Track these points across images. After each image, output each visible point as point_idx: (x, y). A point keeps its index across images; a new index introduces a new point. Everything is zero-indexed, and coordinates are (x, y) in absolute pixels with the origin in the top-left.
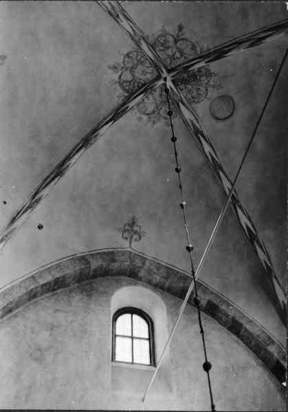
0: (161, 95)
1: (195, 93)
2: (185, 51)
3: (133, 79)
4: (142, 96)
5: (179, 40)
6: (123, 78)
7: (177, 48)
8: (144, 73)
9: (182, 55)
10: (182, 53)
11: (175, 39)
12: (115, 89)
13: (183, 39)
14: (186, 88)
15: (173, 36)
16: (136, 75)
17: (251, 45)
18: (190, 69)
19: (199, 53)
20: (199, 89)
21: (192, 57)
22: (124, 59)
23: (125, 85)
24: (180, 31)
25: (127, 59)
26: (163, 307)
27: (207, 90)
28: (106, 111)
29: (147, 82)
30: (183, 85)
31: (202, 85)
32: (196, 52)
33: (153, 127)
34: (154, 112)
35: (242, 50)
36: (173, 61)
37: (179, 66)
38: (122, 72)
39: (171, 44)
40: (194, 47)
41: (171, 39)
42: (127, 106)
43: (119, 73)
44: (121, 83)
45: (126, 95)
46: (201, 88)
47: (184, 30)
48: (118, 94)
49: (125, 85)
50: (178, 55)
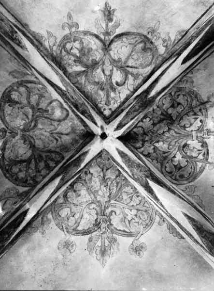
2: (130, 63)
3: (33, 154)
5: (112, 42)
7: (114, 62)
9: (127, 73)
13: (120, 36)
14: (155, 149)
15: (97, 37)
20: (185, 145)
21: (149, 69)
23: (15, 169)
24: (111, 20)
31: (189, 136)
34: (97, 224)
36: (112, 95)
41: (94, 44)
42: (89, 148)
50: (118, 76)
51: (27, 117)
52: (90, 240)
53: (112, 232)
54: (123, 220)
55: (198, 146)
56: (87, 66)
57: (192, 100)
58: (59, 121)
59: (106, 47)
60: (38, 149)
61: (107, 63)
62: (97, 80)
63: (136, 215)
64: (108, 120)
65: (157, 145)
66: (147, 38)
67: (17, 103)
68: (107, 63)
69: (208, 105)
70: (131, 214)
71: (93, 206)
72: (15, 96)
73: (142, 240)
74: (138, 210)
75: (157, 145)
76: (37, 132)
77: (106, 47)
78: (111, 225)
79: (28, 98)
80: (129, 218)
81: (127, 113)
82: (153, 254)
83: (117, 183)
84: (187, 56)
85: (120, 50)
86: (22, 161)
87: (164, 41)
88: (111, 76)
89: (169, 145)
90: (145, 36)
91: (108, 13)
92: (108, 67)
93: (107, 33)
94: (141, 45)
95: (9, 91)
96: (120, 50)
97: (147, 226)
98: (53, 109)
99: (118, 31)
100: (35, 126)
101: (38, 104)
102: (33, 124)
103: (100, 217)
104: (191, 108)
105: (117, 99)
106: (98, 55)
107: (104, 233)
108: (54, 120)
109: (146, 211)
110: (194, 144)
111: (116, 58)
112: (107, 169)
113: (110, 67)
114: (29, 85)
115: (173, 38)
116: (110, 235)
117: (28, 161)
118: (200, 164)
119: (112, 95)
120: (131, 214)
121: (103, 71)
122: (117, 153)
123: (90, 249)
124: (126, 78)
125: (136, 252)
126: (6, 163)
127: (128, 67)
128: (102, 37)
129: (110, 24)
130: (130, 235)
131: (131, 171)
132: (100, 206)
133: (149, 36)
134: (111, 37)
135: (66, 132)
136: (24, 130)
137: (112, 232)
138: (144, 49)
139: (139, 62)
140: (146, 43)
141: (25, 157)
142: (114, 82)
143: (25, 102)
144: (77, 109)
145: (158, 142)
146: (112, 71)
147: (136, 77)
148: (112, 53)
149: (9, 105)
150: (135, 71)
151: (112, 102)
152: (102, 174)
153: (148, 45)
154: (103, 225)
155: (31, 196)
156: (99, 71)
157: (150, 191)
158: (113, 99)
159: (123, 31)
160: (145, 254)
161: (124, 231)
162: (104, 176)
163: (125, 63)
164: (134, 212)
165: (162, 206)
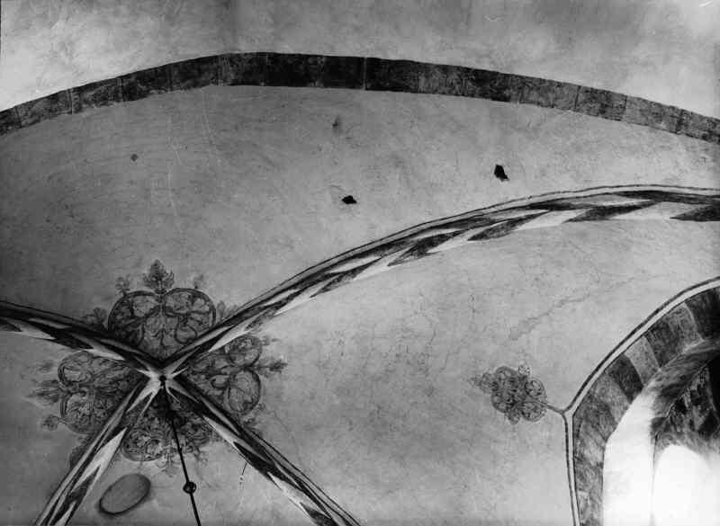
0: (116, 381)
1: (146, 439)
2: (233, 391)
3: (139, 318)
4: (120, 358)
5: (252, 372)
6: (139, 299)
7: (234, 375)
8: (161, 334)
9: (223, 388)
10: (227, 386)
11: (252, 365)
12: (108, 298)
13: (258, 380)
14: (153, 419)
15: (256, 360)
16: (151, 321)
17: (314, 514)
18: (207, 419)
19: (246, 419)
20: (157, 442)
21: (228, 408)
22: (184, 290)
23: (124, 309)
24: (271, 369)
25: (186, 295)
26: (131, 65)
27: (159, 456)
28: (611, 473)
29: (141, 347)
30: (155, 411)
31: (166, 443)
32: (244, 413)
33: (30, 396)
34: (70, 383)
35: (297, 501)
36: (203, 377)
37: (199, 391)
38: (150, 294)
39: (239, 361)
40: (249, 405)
41: (249, 358)
42: (149, 368)
43: (146, 289)
44: (127, 301)
45: (105, 324)
46: (160, 444)
47: (277, 375)
48: (96, 301)
49: (124, 309)
50: (220, 380)
51: (178, 309)
52: (54, 381)
53: (63, 397)
54: (78, 404)
55: (157, 451)
56: (229, 354)
57: (201, 440)
58: (175, 336)
59: (248, 368)
60: (145, 322)
61: (232, 370)
62: (216, 362)
63: (84, 415)
64: (180, 379)
65: (156, 419)
66: (255, 405)
67: (193, 303)
68: (232, 370)
69: (196, 452)
70: (85, 410)
71: (89, 376)
72: (199, 301)
73: (61, 426)
74: (90, 416)
75: (156, 419)
76: (163, 319)
77: (248, 368)
78: (72, 394)
79: (197, 312)
80: (80, 409)
81: (187, 398)
82: (47, 437)
83: (115, 392)
84: (245, 449)
85: (245, 381)
86: (132, 311)
87: (253, 420)
88: (220, 374)
89: (156, 429)
90: (256, 403)
91: (277, 367)
92: (228, 371)
93: (259, 368)
94: (249, 399)
95: (204, 298)
96: (245, 381)
97: (75, 427)
98: (185, 331)
99: (261, 377)
100: (169, 316)
101: (192, 319)
102: (170, 314)
103: (77, 384)
104: (192, 440)
105: (199, 381)
106: (239, 361)
107: (62, 391)
108: (176, 330)
109: (90, 424)
110: (160, 448)
111: (237, 377)
112: (128, 381)
113: (228, 373)
114: (211, 315)
115: (256, 427)
116: (61, 395)
117: (133, 316)
118: (140, 456)
119: (203, 377)
120: (85, 410)
121: (225, 367)
122: (148, 393)
123: (46, 384)
124: (219, 389)
125: (47, 421)
126: (130, 299)
127: (230, 389)
128: (257, 363)
129: (268, 370)
130: (63, 413)
131: (132, 411)
132: (90, 381)
133: (257, 406)
134: (257, 372)
135: (164, 342)
136: (164, 307)
137: (63, 397)
138: (246, 403)
139: (234, 398)
140: (249, 405)
141: (137, 313)
142: (214, 378)
143: (195, 309)
144: (190, 357)
145: (159, 419)
146: (226, 374)
147: (221, 397)
148: (242, 372)
149: (189, 297)
150: (226, 395)
151: (196, 377)
152: (122, 377)
153: (249, 406)
154: (70, 389)
155: (104, 341)
156: (226, 364)
157: (115, 433)
158: (199, 377)
159: (262, 382)
160: (46, 430)
161: (66, 407)
162: (121, 380)
163: (234, 386)
164: (87, 412)
165: (103, 445)
